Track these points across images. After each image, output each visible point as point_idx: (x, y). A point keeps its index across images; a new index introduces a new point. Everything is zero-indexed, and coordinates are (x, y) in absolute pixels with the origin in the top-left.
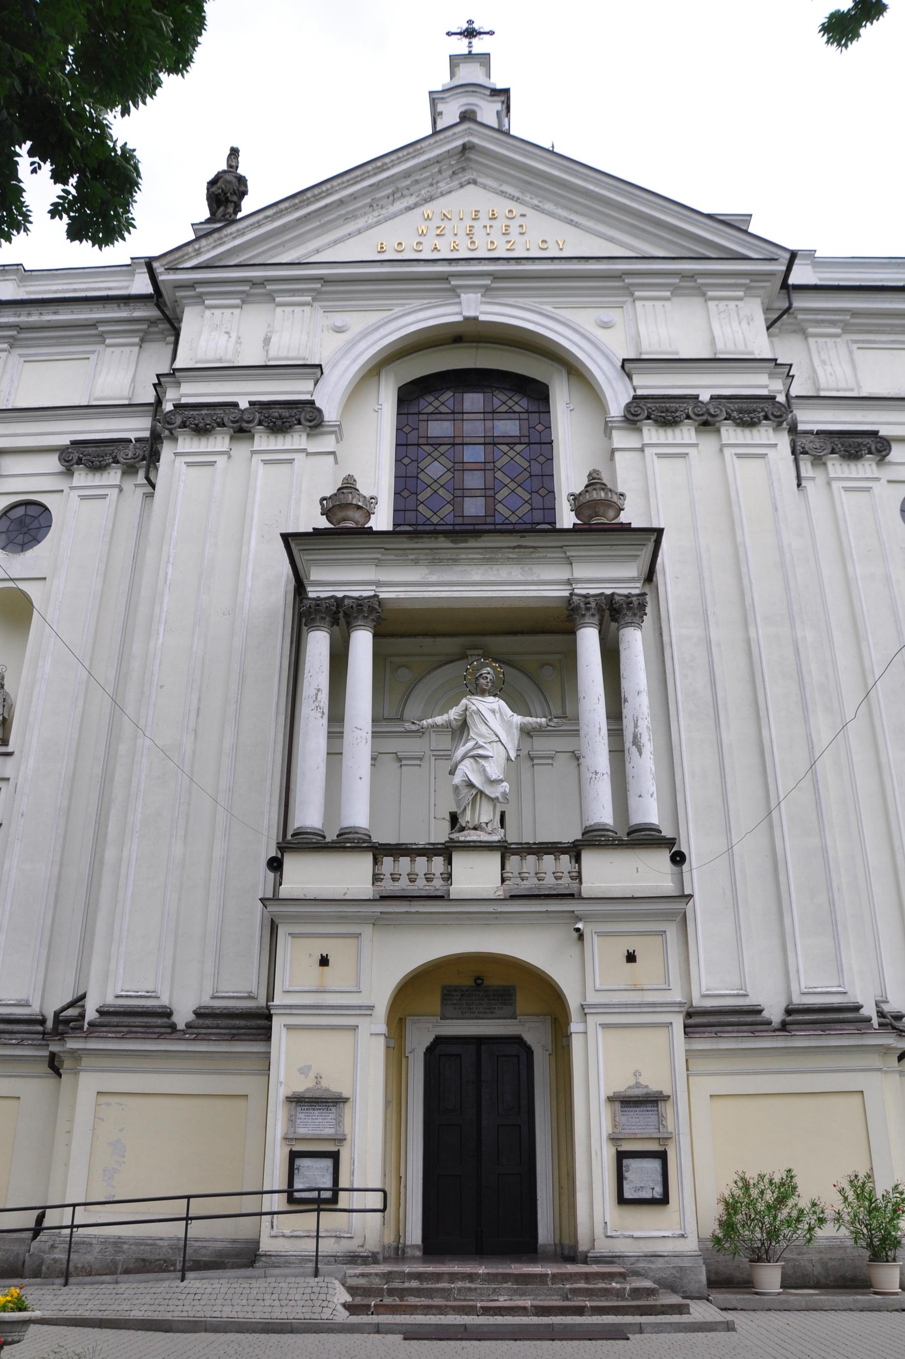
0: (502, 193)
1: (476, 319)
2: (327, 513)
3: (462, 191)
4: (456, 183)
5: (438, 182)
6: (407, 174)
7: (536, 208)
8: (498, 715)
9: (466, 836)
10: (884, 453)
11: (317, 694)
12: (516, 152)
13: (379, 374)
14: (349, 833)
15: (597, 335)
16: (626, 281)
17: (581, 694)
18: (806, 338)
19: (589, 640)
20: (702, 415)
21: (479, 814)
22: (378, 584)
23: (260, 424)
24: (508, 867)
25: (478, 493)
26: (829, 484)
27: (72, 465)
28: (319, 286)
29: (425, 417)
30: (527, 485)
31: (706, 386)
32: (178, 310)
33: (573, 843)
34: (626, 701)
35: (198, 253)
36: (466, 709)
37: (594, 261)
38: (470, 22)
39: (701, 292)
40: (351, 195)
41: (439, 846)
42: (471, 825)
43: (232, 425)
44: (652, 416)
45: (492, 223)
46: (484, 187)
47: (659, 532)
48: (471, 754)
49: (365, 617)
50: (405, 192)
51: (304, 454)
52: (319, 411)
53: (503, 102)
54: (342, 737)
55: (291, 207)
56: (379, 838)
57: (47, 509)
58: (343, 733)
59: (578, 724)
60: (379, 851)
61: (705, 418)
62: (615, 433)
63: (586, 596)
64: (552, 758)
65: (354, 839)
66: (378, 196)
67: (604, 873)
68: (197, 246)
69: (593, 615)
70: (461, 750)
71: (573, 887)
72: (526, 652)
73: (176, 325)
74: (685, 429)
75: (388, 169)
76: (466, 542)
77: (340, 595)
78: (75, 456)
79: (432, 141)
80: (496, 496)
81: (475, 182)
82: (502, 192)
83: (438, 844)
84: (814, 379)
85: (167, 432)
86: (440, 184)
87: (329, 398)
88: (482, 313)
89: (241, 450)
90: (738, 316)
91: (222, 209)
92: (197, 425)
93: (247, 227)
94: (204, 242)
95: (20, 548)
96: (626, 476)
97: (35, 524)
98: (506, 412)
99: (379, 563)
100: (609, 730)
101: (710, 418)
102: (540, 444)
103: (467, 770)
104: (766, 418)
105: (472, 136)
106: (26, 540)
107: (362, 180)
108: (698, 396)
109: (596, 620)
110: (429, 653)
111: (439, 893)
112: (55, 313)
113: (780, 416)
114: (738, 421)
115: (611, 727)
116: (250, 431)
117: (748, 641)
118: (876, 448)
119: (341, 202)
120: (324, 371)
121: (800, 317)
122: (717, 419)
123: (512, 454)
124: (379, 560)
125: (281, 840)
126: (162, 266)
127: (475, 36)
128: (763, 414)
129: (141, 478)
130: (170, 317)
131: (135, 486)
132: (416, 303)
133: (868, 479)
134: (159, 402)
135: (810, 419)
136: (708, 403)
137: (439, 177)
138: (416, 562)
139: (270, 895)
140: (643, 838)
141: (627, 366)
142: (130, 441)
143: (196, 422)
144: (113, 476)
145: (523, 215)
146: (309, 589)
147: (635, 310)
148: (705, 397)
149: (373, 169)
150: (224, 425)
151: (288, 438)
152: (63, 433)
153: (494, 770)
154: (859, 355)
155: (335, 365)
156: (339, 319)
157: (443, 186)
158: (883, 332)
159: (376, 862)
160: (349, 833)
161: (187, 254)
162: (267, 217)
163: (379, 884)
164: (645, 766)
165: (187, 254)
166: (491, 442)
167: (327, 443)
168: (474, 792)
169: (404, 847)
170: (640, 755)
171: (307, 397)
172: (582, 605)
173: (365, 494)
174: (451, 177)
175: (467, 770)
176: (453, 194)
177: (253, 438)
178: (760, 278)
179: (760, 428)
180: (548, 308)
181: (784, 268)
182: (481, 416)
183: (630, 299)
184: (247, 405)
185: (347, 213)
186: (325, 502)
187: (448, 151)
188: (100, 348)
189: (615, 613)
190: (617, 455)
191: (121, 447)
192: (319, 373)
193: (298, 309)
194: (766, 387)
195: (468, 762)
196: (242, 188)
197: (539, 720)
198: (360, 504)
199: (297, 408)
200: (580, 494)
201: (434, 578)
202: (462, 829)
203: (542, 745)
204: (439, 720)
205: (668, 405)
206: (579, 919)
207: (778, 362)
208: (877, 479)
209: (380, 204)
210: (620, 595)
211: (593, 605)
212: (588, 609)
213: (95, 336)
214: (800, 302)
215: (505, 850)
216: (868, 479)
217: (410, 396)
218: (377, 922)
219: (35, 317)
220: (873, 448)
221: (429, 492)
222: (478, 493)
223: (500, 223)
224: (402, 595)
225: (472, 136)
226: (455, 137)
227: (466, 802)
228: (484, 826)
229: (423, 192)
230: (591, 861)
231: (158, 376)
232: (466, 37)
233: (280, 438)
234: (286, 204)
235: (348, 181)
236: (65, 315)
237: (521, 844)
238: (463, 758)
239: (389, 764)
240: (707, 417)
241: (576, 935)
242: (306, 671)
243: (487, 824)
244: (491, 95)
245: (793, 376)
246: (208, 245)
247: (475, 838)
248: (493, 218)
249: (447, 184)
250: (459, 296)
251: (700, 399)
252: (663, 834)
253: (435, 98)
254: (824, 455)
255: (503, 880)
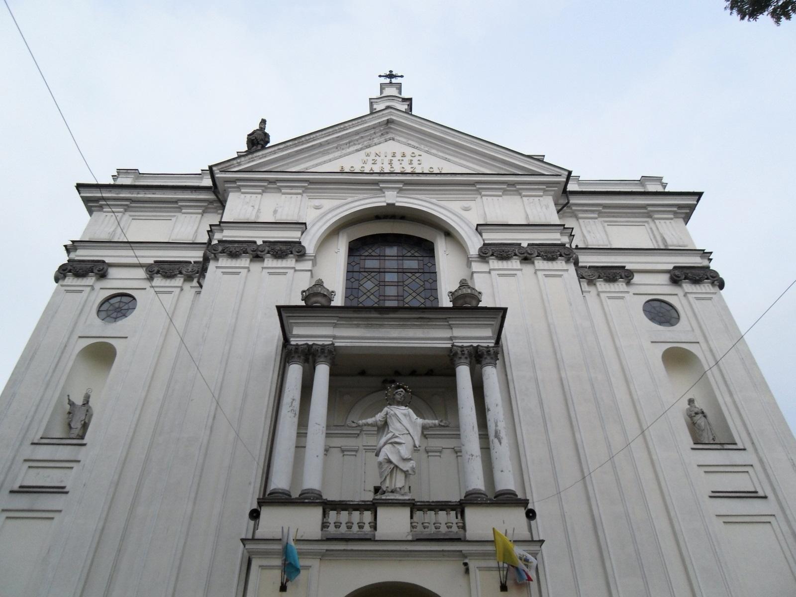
0: (409, 145)
1: (393, 205)
2: (305, 299)
3: (386, 143)
4: (383, 139)
5: (373, 138)
6: (357, 133)
7: (427, 152)
8: (408, 418)
9: (386, 496)
10: (630, 278)
11: (292, 402)
12: (416, 124)
13: (338, 234)
14: (308, 493)
15: (461, 213)
16: (477, 186)
17: (460, 415)
18: (578, 220)
19: (463, 373)
20: (523, 254)
21: (396, 480)
22: (334, 337)
23: (268, 253)
24: (415, 519)
25: (394, 298)
26: (598, 295)
27: (154, 274)
28: (307, 185)
29: (363, 258)
30: (423, 294)
31: (525, 239)
32: (226, 195)
33: (459, 502)
34: (489, 410)
35: (239, 164)
36: (387, 414)
37: (459, 175)
38: (391, 71)
39: (518, 193)
40: (327, 141)
41: (368, 503)
42: (389, 490)
43: (251, 252)
44: (495, 254)
45: (403, 158)
46: (399, 141)
47: (505, 310)
48: (390, 441)
49: (326, 357)
50: (356, 142)
51: (293, 270)
52: (304, 247)
53: (408, 105)
54: (306, 437)
55: (293, 145)
56: (331, 495)
57: (134, 299)
58: (306, 433)
59: (459, 430)
60: (328, 506)
61: (525, 255)
62: (473, 264)
63: (462, 347)
64: (440, 452)
65: (311, 497)
66: (341, 143)
67: (481, 522)
68: (239, 161)
69: (466, 358)
70: (384, 440)
71: (461, 536)
72: (427, 381)
73: (224, 204)
74: (514, 261)
75: (347, 129)
76: (388, 314)
77: (310, 343)
78: (156, 269)
79: (371, 117)
80: (405, 300)
81: (393, 139)
82: (409, 144)
83: (368, 501)
84: (584, 241)
85: (213, 255)
86: (374, 140)
87: (309, 243)
88: (397, 202)
89: (256, 267)
90: (540, 205)
91: (255, 147)
92: (231, 252)
93: (268, 153)
94: (243, 159)
95: (114, 320)
96: (480, 283)
97: (126, 307)
98: (410, 256)
99: (335, 326)
100: (479, 435)
101: (528, 255)
102: (430, 274)
103: (387, 451)
104: (561, 255)
105: (391, 115)
106: (119, 315)
107: (333, 134)
108: (521, 243)
109: (468, 361)
110: (364, 382)
111: (368, 537)
112: (153, 194)
113: (569, 255)
114: (545, 257)
115: (481, 433)
116: (262, 257)
117: (561, 380)
118: (625, 276)
119: (321, 145)
120: (307, 227)
121: (574, 208)
122: (532, 256)
123: (414, 278)
124: (336, 324)
125: (261, 497)
126: (218, 169)
127: (393, 78)
128: (559, 253)
129: (195, 283)
130: (221, 199)
131: (189, 289)
132: (361, 196)
133: (622, 292)
134: (210, 240)
135: (586, 260)
136: (526, 248)
137: (374, 136)
138: (358, 326)
139: (250, 537)
140: (507, 500)
141: (480, 228)
142: (190, 262)
143: (231, 250)
144: (178, 281)
145: (419, 155)
146: (291, 339)
147: (483, 202)
148: (525, 244)
149: (339, 129)
150: (247, 253)
151: (284, 261)
152: (150, 257)
153: (405, 451)
154: (609, 229)
155: (314, 225)
156: (317, 202)
157: (376, 140)
158: (621, 217)
159: (325, 514)
160: (308, 493)
161: (233, 165)
162: (279, 149)
163: (326, 529)
164: (502, 452)
165: (233, 165)
166: (402, 271)
167: (307, 265)
168: (392, 466)
169: (344, 503)
170: (500, 443)
171: (298, 240)
172: (459, 352)
173: (328, 288)
174: (380, 136)
175: (387, 451)
176: (381, 145)
177: (263, 260)
178: (551, 185)
179: (557, 261)
180: (434, 201)
181: (565, 180)
182: (396, 258)
183: (479, 196)
184: (262, 243)
185: (324, 151)
186: (304, 293)
187: (379, 123)
188: (178, 214)
189: (478, 358)
190: (475, 275)
191: (184, 265)
192: (305, 228)
193: (294, 196)
194: (559, 240)
195: (388, 447)
196: (267, 140)
197: (434, 421)
198: (325, 293)
199: (290, 245)
200: (456, 291)
201: (368, 335)
202: (384, 492)
203: (435, 443)
204: (370, 421)
205: (503, 248)
206: (465, 556)
207: (565, 227)
208: (628, 292)
209: (342, 147)
210: (482, 347)
211: (466, 352)
212: (463, 354)
213: (177, 208)
214: (574, 200)
215: (414, 506)
216: (622, 292)
217: (355, 248)
218: (323, 556)
219: (142, 195)
220: (623, 275)
221: (365, 297)
222: (394, 298)
223: (407, 160)
224: (349, 344)
225: (391, 115)
226: (383, 116)
227: (386, 473)
228: (399, 490)
229: (365, 143)
230: (471, 514)
231: (211, 226)
232: (388, 78)
233: (280, 261)
234: (290, 143)
235: (325, 134)
236: (159, 195)
237: (424, 502)
238: (385, 444)
239: (336, 454)
240: (527, 256)
241: (463, 568)
242: (286, 388)
243: (400, 488)
244: (403, 101)
245: (574, 235)
246: (245, 161)
247: (392, 497)
248: (404, 155)
249: (378, 139)
250: (384, 193)
251: (522, 245)
252: (519, 497)
253: (372, 102)
254: (594, 279)
255: (413, 527)
